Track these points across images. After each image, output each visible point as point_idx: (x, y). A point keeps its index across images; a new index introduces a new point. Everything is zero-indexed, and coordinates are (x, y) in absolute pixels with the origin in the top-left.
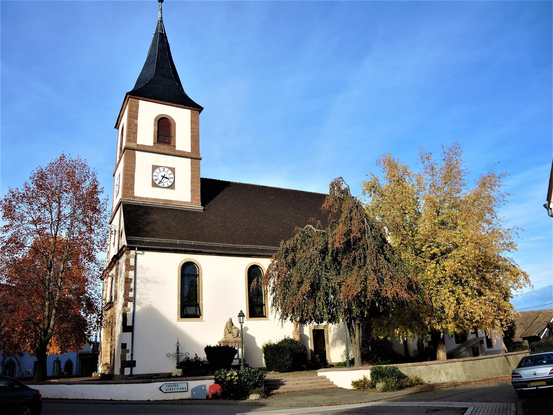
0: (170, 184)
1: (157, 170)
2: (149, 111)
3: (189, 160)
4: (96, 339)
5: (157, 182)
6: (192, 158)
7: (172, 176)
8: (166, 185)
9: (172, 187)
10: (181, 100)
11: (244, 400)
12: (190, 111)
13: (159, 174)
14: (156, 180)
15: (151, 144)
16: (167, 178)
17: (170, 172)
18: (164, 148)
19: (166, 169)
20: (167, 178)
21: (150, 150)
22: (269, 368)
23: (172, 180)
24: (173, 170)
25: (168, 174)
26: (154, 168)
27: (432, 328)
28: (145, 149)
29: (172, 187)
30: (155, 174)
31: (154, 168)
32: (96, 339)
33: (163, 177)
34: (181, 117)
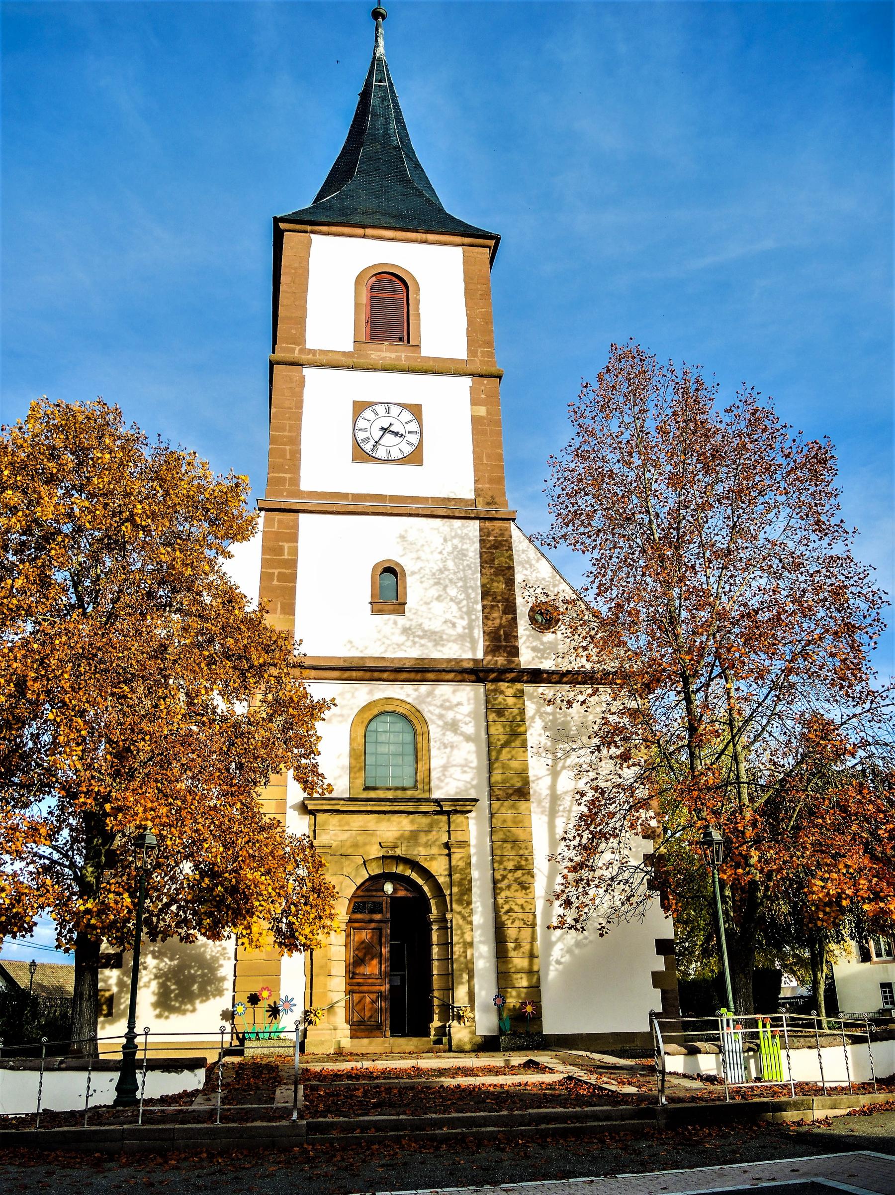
0: (407, 450)
1: (368, 414)
2: (336, 266)
3: (467, 381)
4: (877, 943)
5: (368, 447)
6: (474, 375)
7: (414, 426)
8: (396, 454)
9: (415, 458)
10: (423, 217)
11: (600, 1095)
12: (460, 250)
13: (371, 424)
14: (367, 439)
15: (348, 346)
16: (396, 434)
17: (406, 416)
18: (384, 352)
19: (395, 410)
20: (396, 434)
21: (344, 361)
22: (690, 1007)
23: (414, 439)
24: (416, 411)
25: (402, 421)
26: (359, 407)
27: (753, 829)
28: (331, 362)
29: (415, 458)
30: (361, 424)
31: (359, 407)
32: (877, 943)
33: (384, 430)
34: (437, 271)
